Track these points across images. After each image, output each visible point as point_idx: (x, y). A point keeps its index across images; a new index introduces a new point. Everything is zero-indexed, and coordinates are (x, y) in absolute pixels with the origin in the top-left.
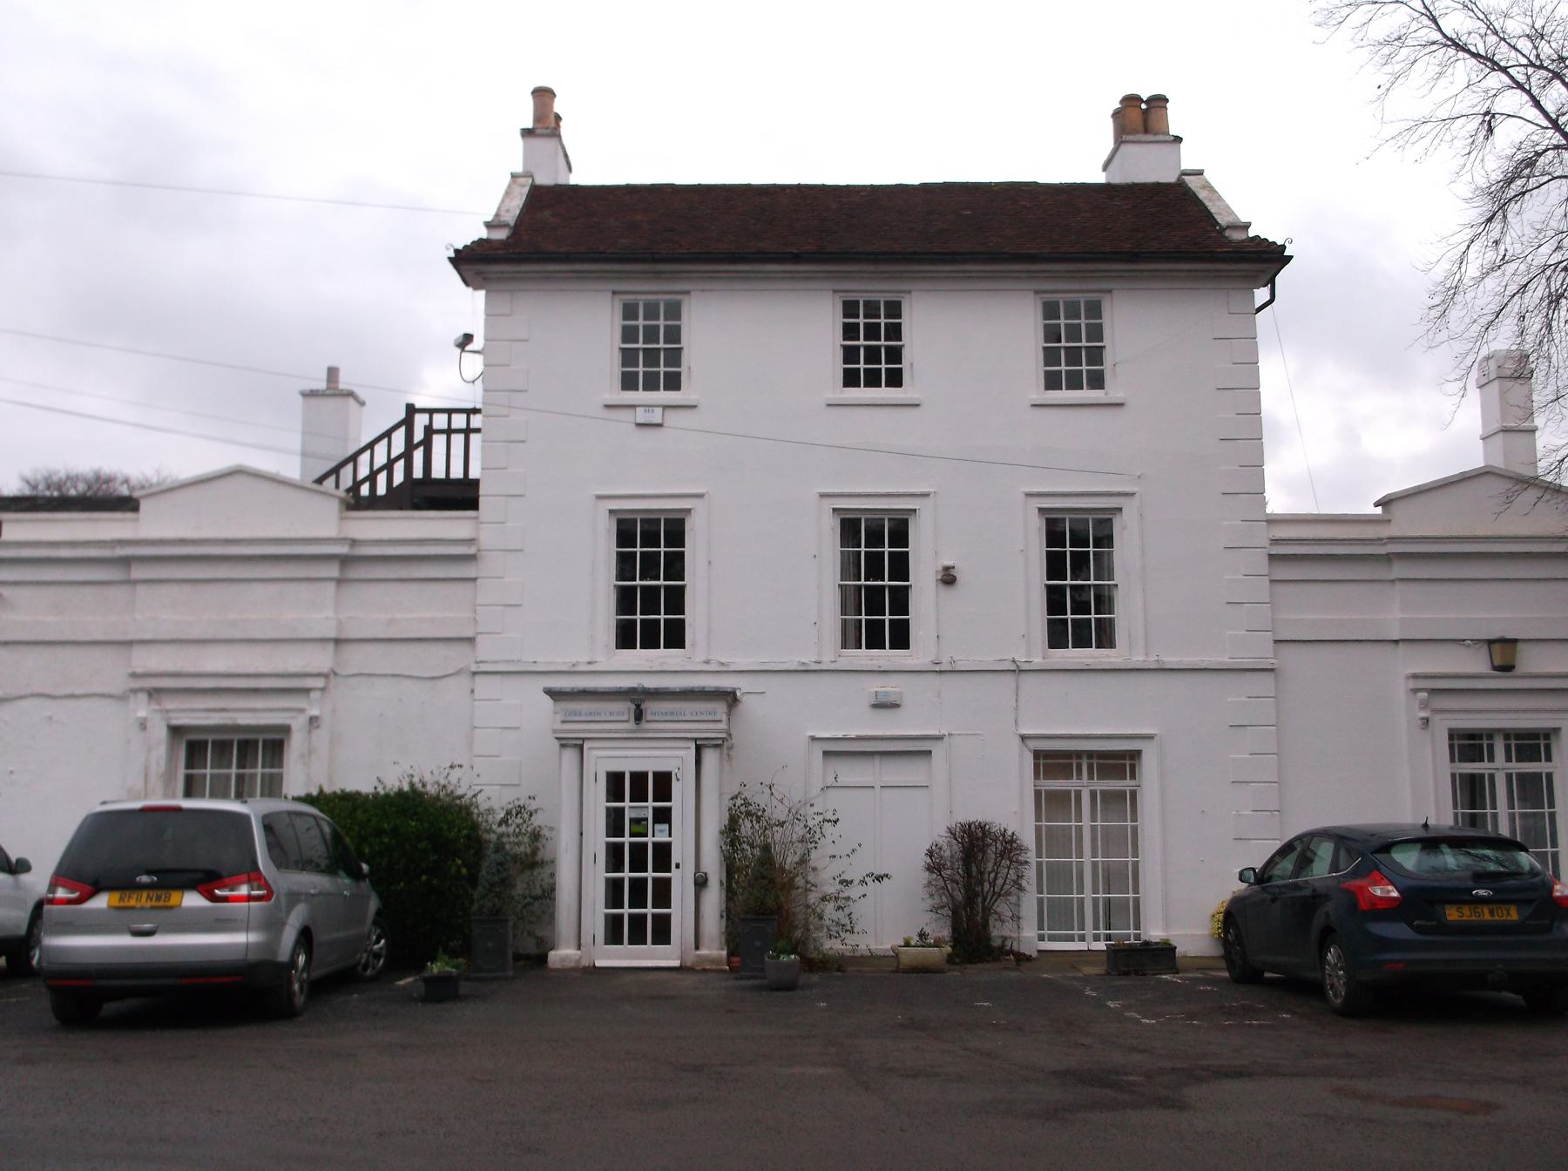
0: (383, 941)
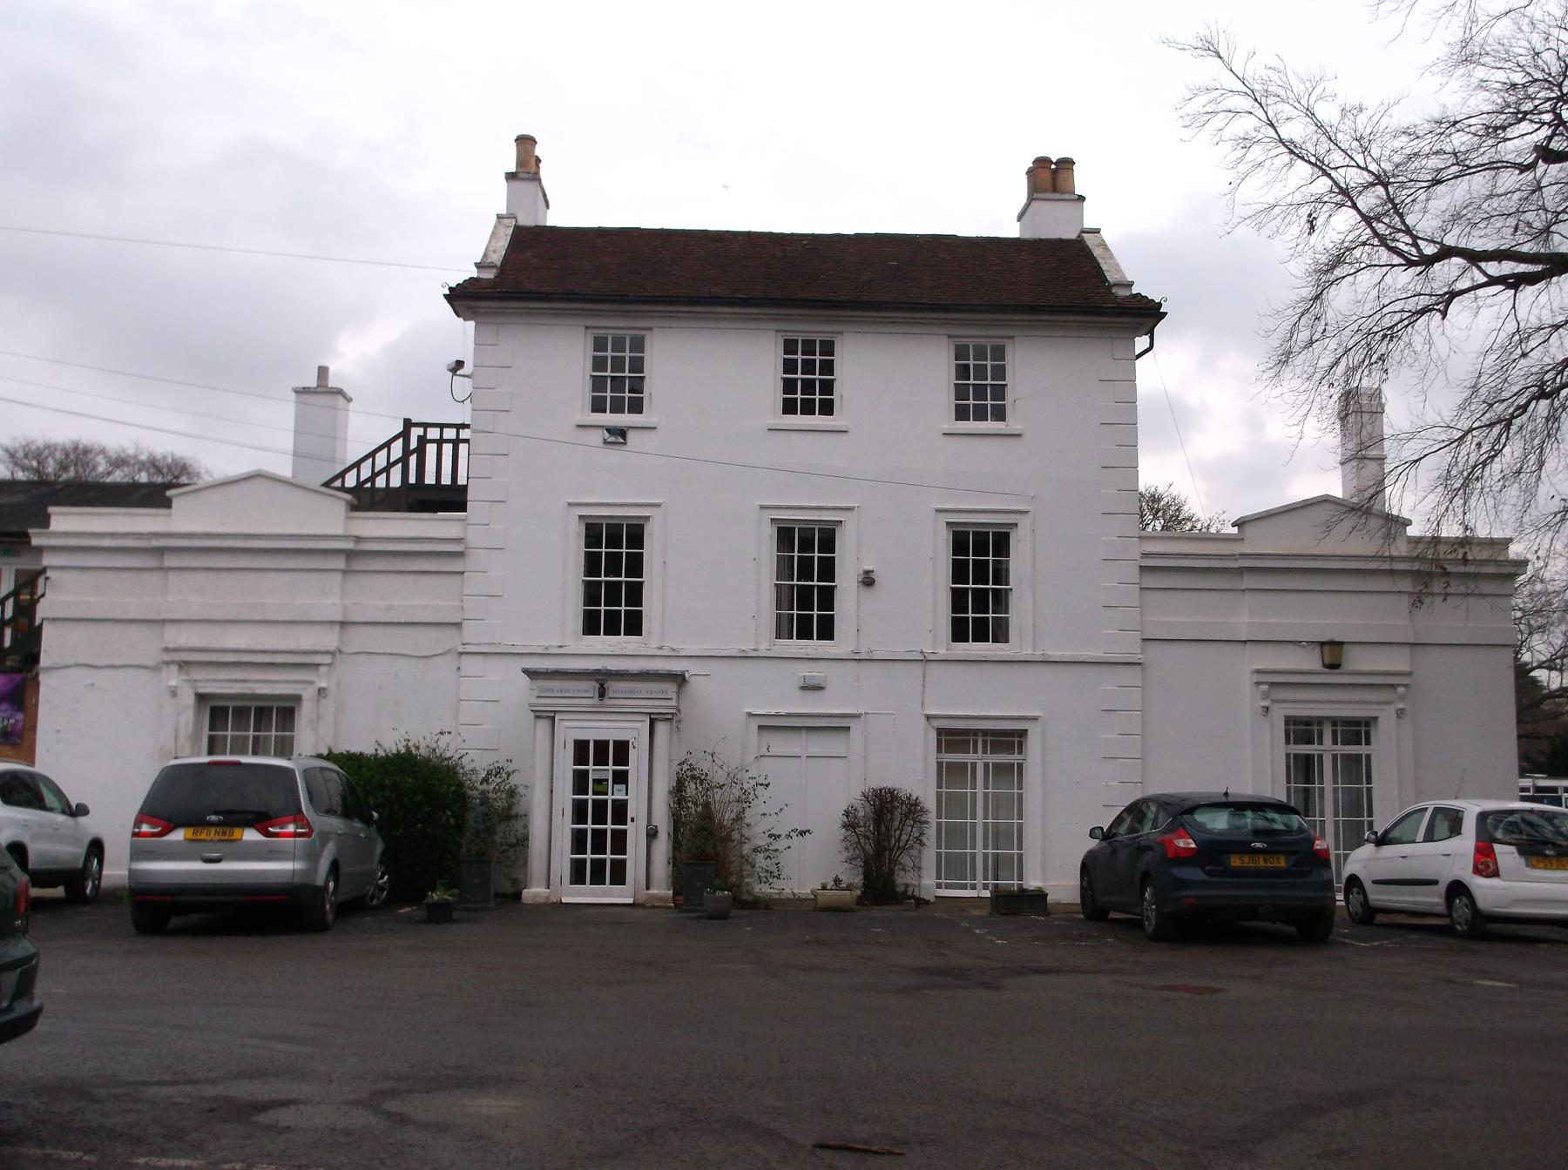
0: (386, 877)
